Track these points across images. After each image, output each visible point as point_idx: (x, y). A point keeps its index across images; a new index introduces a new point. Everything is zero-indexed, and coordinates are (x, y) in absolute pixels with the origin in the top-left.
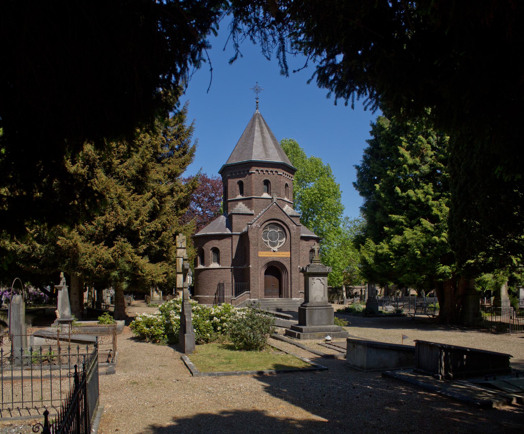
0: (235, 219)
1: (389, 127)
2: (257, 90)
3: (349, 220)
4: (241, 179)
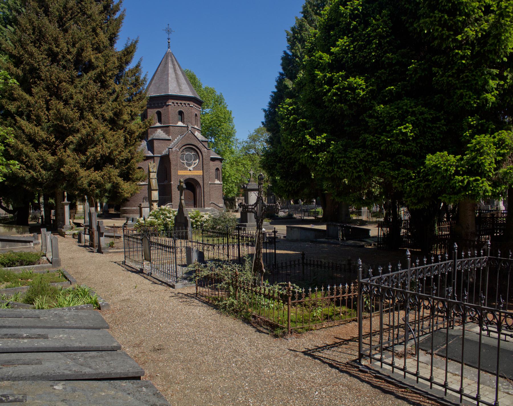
0: (156, 143)
1: (292, 87)
3: (238, 141)
4: (159, 110)
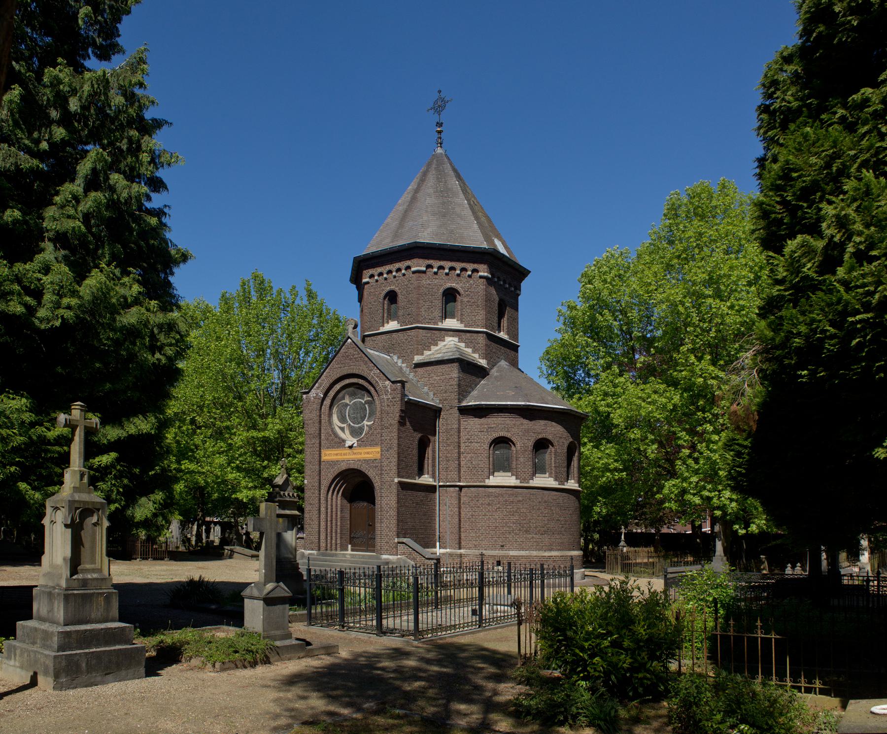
2: (439, 107)
